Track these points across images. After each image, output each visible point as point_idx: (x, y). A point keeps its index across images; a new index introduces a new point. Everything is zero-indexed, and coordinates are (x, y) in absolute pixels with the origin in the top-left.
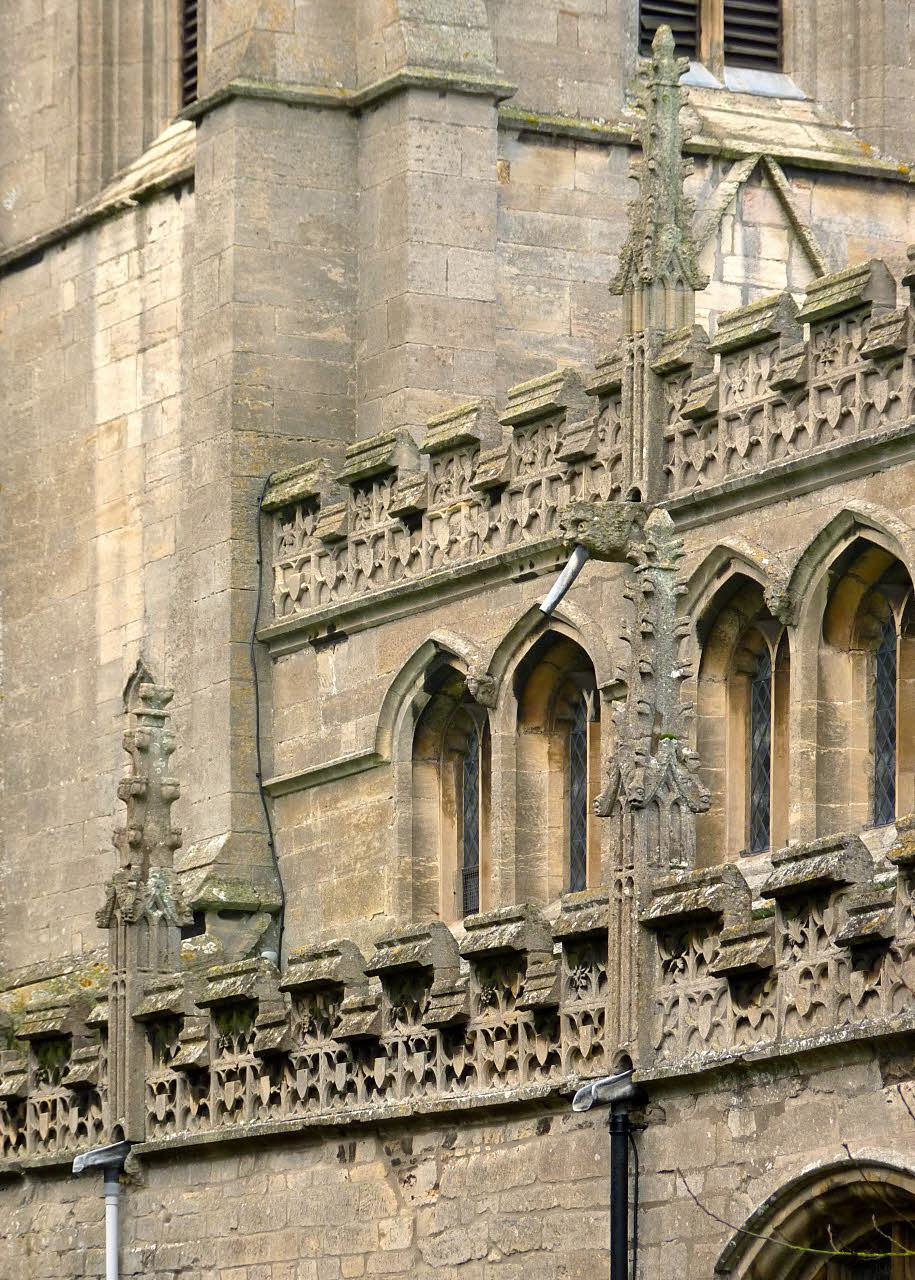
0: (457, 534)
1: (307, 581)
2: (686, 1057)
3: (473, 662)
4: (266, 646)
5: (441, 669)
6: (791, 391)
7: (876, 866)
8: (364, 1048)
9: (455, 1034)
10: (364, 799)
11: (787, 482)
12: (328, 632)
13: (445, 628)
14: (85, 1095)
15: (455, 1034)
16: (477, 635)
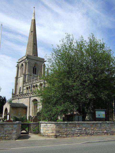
0: (28, 84)
1: (24, 85)
2: (31, 96)
3: (28, 87)
4: (23, 87)
5: (27, 87)
6: (28, 95)
7: (106, 64)
8: (24, 96)
9: (24, 96)
10: (25, 90)
11: (35, 83)
12: (25, 86)
13: (27, 86)
14: (18, 97)
15: (26, 96)
16: (28, 86)
